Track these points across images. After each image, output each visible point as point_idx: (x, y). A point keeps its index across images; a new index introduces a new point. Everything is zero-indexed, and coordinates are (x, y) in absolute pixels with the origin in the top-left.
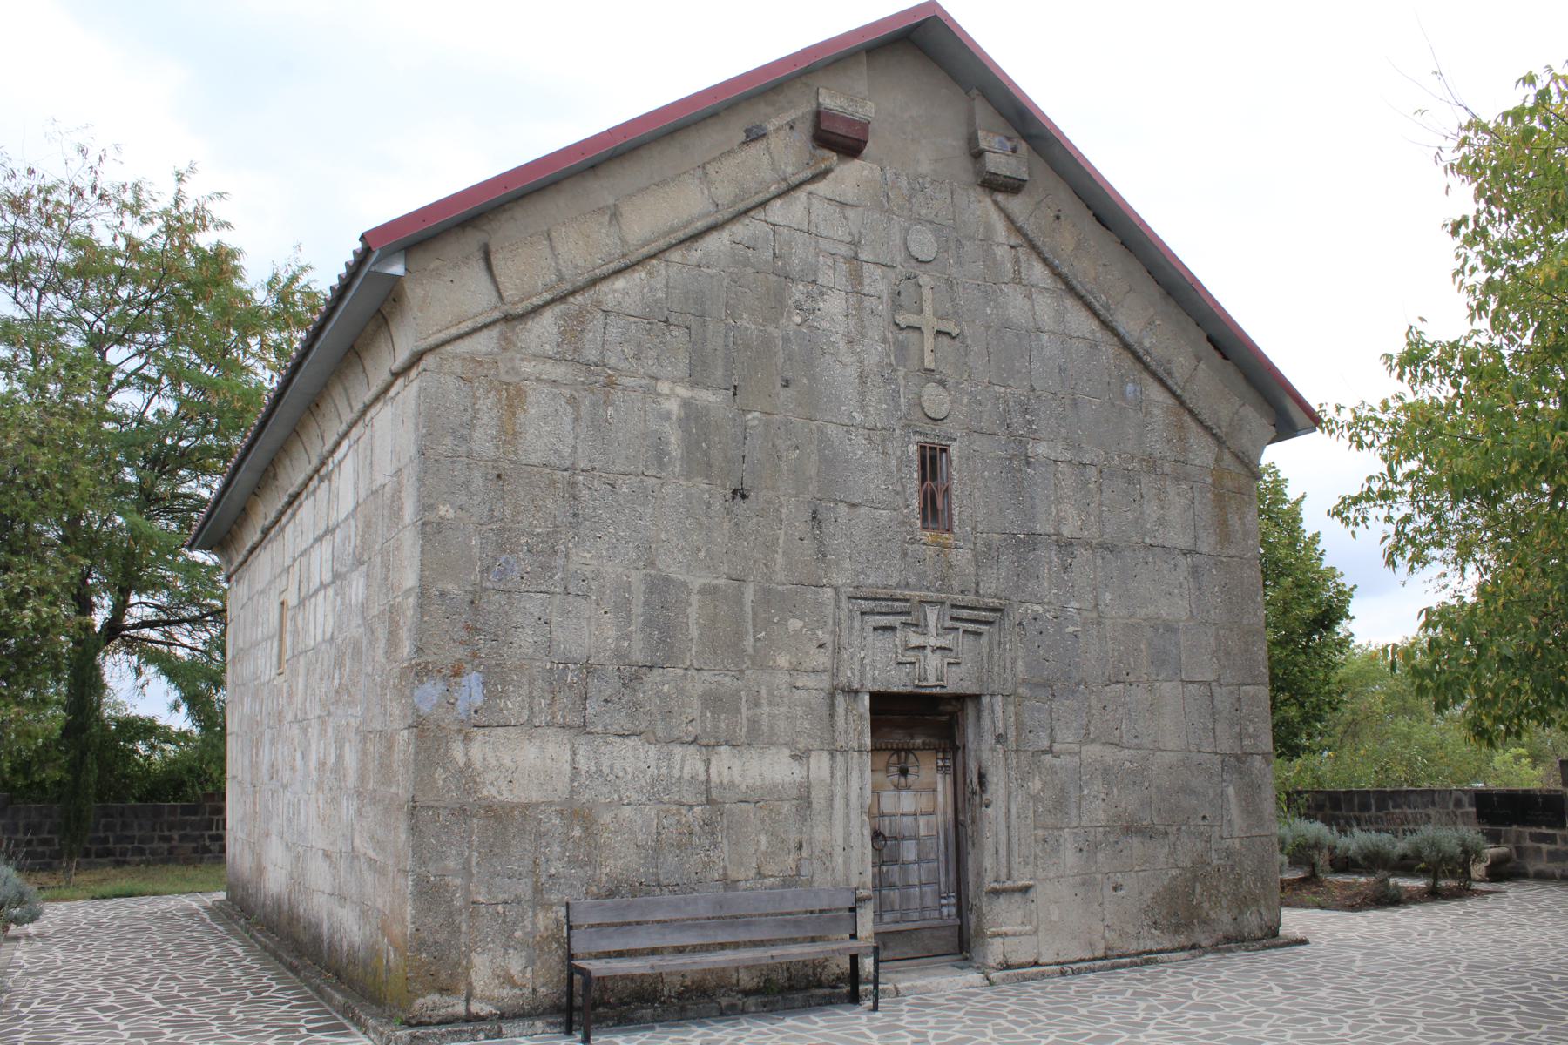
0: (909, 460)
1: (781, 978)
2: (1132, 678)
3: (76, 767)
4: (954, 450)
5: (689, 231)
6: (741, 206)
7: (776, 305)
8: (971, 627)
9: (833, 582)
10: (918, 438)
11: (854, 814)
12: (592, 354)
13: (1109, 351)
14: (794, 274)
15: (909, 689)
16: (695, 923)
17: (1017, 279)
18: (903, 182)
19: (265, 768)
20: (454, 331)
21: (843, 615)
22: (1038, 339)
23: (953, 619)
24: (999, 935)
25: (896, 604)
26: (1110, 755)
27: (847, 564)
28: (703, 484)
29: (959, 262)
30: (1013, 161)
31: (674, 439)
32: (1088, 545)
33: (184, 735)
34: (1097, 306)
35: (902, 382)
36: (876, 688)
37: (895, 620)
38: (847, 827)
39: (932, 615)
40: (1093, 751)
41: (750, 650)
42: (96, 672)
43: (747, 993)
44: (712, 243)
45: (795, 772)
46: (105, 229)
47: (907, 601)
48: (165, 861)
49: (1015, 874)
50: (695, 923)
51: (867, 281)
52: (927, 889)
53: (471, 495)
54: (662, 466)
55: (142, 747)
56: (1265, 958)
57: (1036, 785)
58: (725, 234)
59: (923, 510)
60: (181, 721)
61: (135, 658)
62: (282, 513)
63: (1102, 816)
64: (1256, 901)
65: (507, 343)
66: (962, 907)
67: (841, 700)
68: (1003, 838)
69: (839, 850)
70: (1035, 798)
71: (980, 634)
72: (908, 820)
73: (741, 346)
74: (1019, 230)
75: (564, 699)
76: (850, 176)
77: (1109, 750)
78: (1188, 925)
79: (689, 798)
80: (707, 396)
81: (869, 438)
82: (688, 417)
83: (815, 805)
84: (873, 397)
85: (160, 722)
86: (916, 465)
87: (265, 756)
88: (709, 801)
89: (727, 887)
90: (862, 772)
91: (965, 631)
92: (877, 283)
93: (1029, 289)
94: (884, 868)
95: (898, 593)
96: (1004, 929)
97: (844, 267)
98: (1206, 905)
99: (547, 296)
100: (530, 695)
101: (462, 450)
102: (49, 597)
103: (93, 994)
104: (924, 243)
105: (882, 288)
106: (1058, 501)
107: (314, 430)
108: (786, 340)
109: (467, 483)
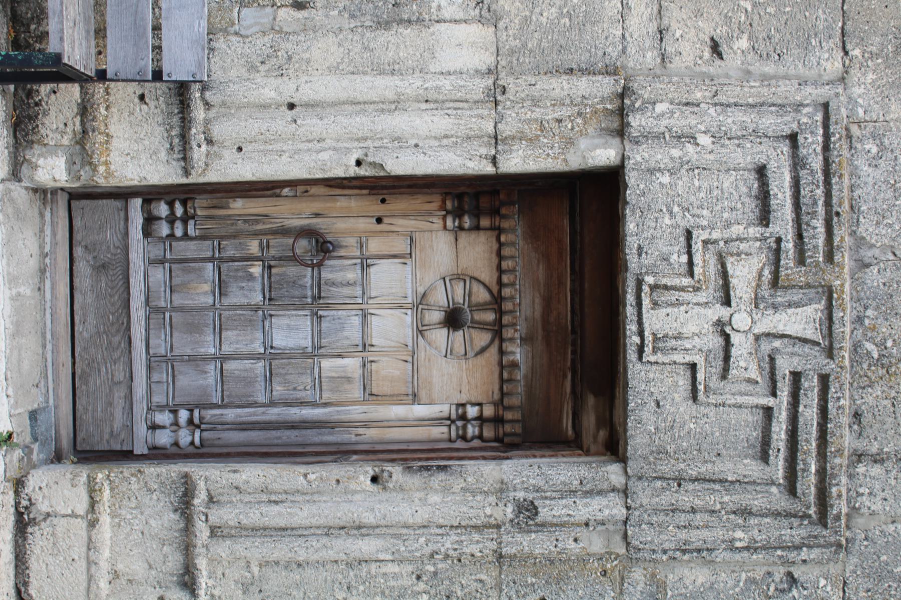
9: (855, 74)
11: (360, 123)
15: (633, 262)
21: (786, 90)
23: (796, 377)
24: (93, 504)
25: (819, 224)
36: (632, 178)
37: (783, 223)
39: (801, 320)
47: (830, 257)
49: (223, 549)
52: (210, 378)
67: (603, 88)
68: (302, 515)
69: (288, 89)
71: (764, 457)
83: (383, 37)
91: (768, 412)
94: (256, 269)
95: (841, 233)
96: (105, 520)
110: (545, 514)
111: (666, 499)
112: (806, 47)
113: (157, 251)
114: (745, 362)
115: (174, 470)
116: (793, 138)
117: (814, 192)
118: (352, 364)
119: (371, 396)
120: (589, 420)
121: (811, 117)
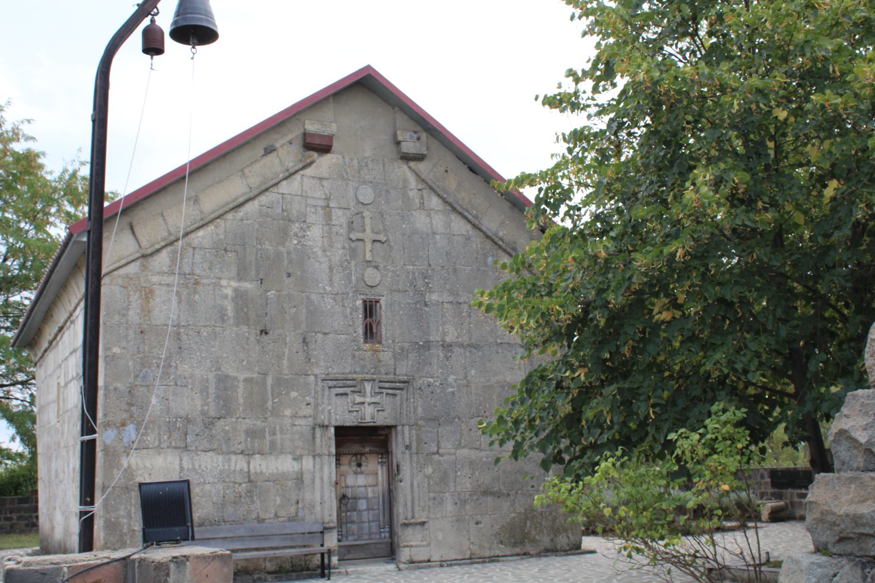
10: (362, 297)
18: (355, 162)
21: (319, 389)
23: (380, 388)
24: (408, 546)
25: (348, 382)
35: (353, 268)
36: (337, 424)
41: (270, 408)
49: (417, 516)
51: (334, 218)
52: (373, 524)
63: (468, 486)
67: (318, 432)
68: (409, 498)
69: (318, 504)
77: (473, 452)
84: (336, 278)
91: (387, 394)
92: (340, 218)
94: (349, 514)
95: (350, 376)
97: (320, 211)
105: (343, 221)
110: (408, 443)
111: (405, 417)
112: (308, 384)
113: (344, 539)
114: (377, 399)
115: (398, 529)
116: (330, 388)
117: (341, 383)
118: (370, 489)
119: (376, 485)
120: (383, 432)
121: (326, 383)
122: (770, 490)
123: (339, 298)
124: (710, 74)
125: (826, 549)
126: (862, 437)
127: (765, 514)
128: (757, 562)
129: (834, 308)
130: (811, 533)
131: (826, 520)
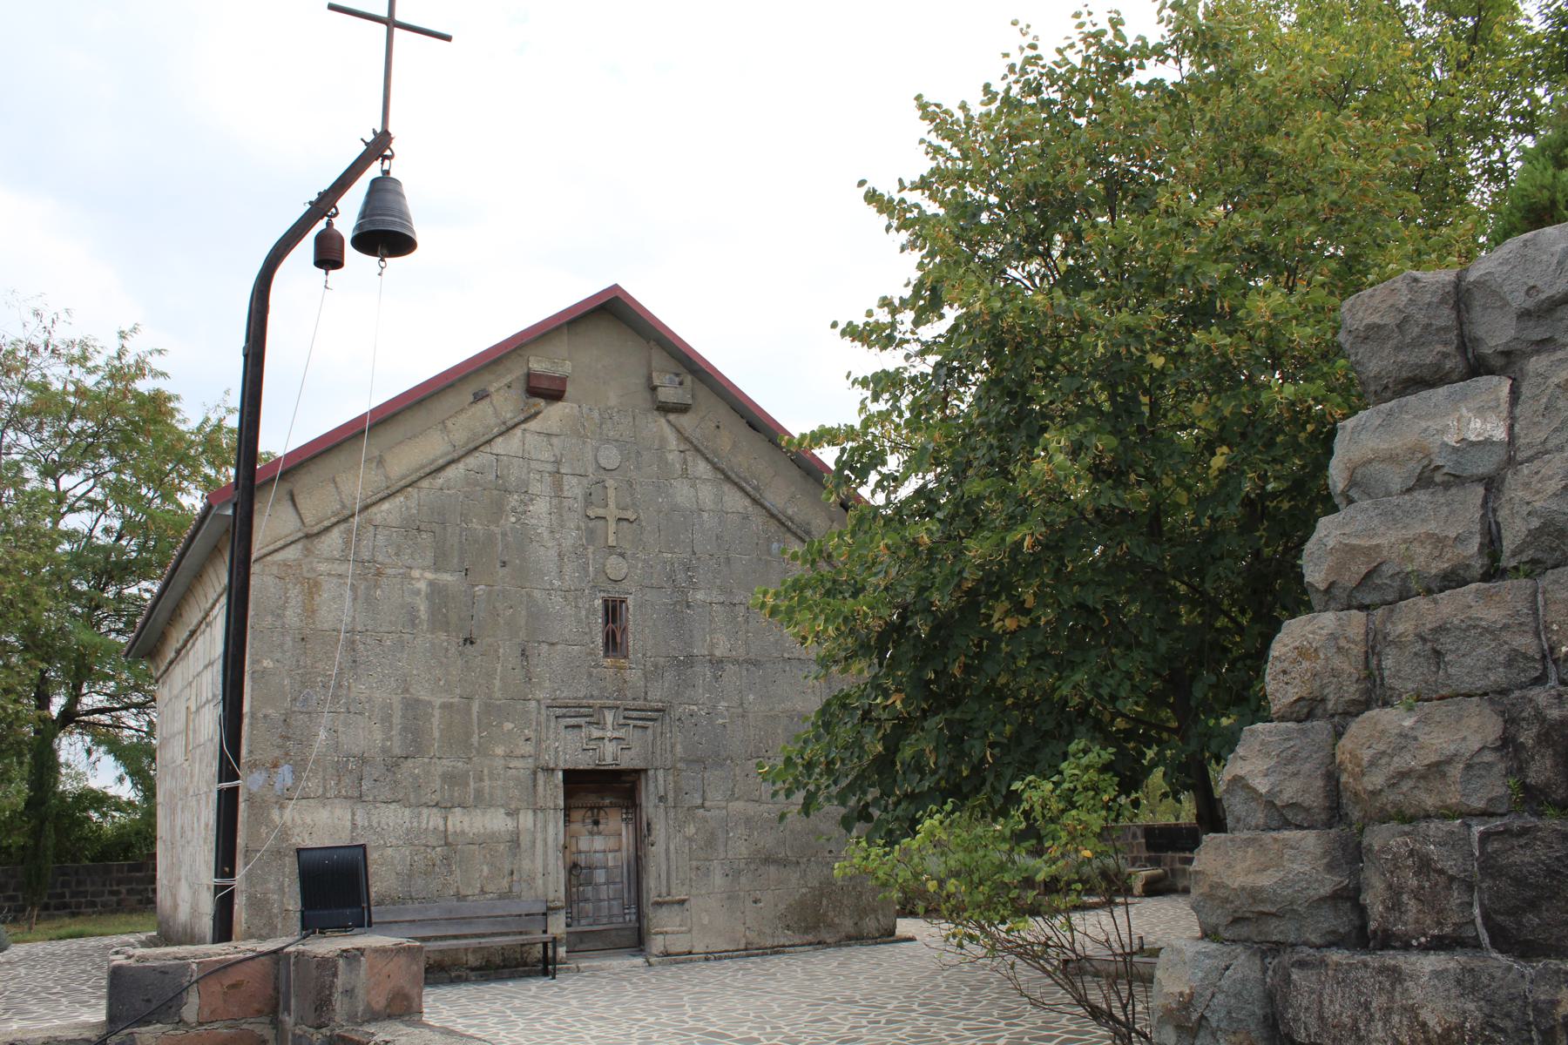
0: (595, 611)
1: (498, 960)
2: (770, 754)
3: (37, 834)
4: (630, 601)
5: (433, 467)
6: (471, 446)
7: (498, 510)
8: (640, 723)
12: (366, 555)
13: (758, 520)
14: (511, 488)
16: (433, 922)
17: (684, 473)
18: (596, 414)
19: (178, 830)
20: (272, 548)
21: (543, 719)
22: (700, 516)
26: (752, 809)
27: (547, 684)
28: (443, 636)
29: (638, 468)
30: (680, 391)
31: (423, 608)
32: (736, 661)
33: (130, 803)
34: (749, 489)
38: (545, 860)
40: (738, 805)
42: (53, 754)
43: (473, 969)
44: (451, 472)
45: (510, 824)
46: (58, 375)
48: (114, 912)
49: (673, 891)
50: (433, 922)
53: (284, 652)
54: (414, 625)
55: (95, 816)
56: (885, 950)
57: (691, 830)
58: (461, 466)
59: (606, 644)
60: (126, 791)
61: (88, 739)
62: (186, 642)
63: (745, 852)
64: (874, 911)
65: (308, 552)
66: (640, 915)
67: (541, 776)
68: (664, 867)
70: (690, 839)
72: (600, 856)
73: (472, 541)
74: (687, 439)
75: (346, 780)
76: (554, 415)
77: (750, 805)
78: (816, 927)
79: (433, 841)
80: (447, 577)
81: (565, 598)
82: (432, 592)
84: (568, 569)
85: (111, 792)
86: (601, 613)
87: (178, 823)
88: (446, 844)
89: (459, 900)
90: (556, 826)
92: (574, 488)
93: (693, 481)
97: (548, 479)
98: (831, 914)
99: (334, 520)
100: (324, 779)
101: (278, 624)
102: (14, 697)
103: (46, 988)
104: (610, 457)
105: (578, 492)
106: (713, 631)
107: (199, 591)
108: (504, 534)
109: (281, 645)
115: (649, 910)
119: (619, 850)
122: (1145, 854)
123: (570, 596)
124: (1068, 306)
125: (1216, 933)
126: (1262, 786)
127: (1138, 886)
128: (1128, 950)
129: (1227, 614)
130: (1197, 912)
131: (1215, 896)
